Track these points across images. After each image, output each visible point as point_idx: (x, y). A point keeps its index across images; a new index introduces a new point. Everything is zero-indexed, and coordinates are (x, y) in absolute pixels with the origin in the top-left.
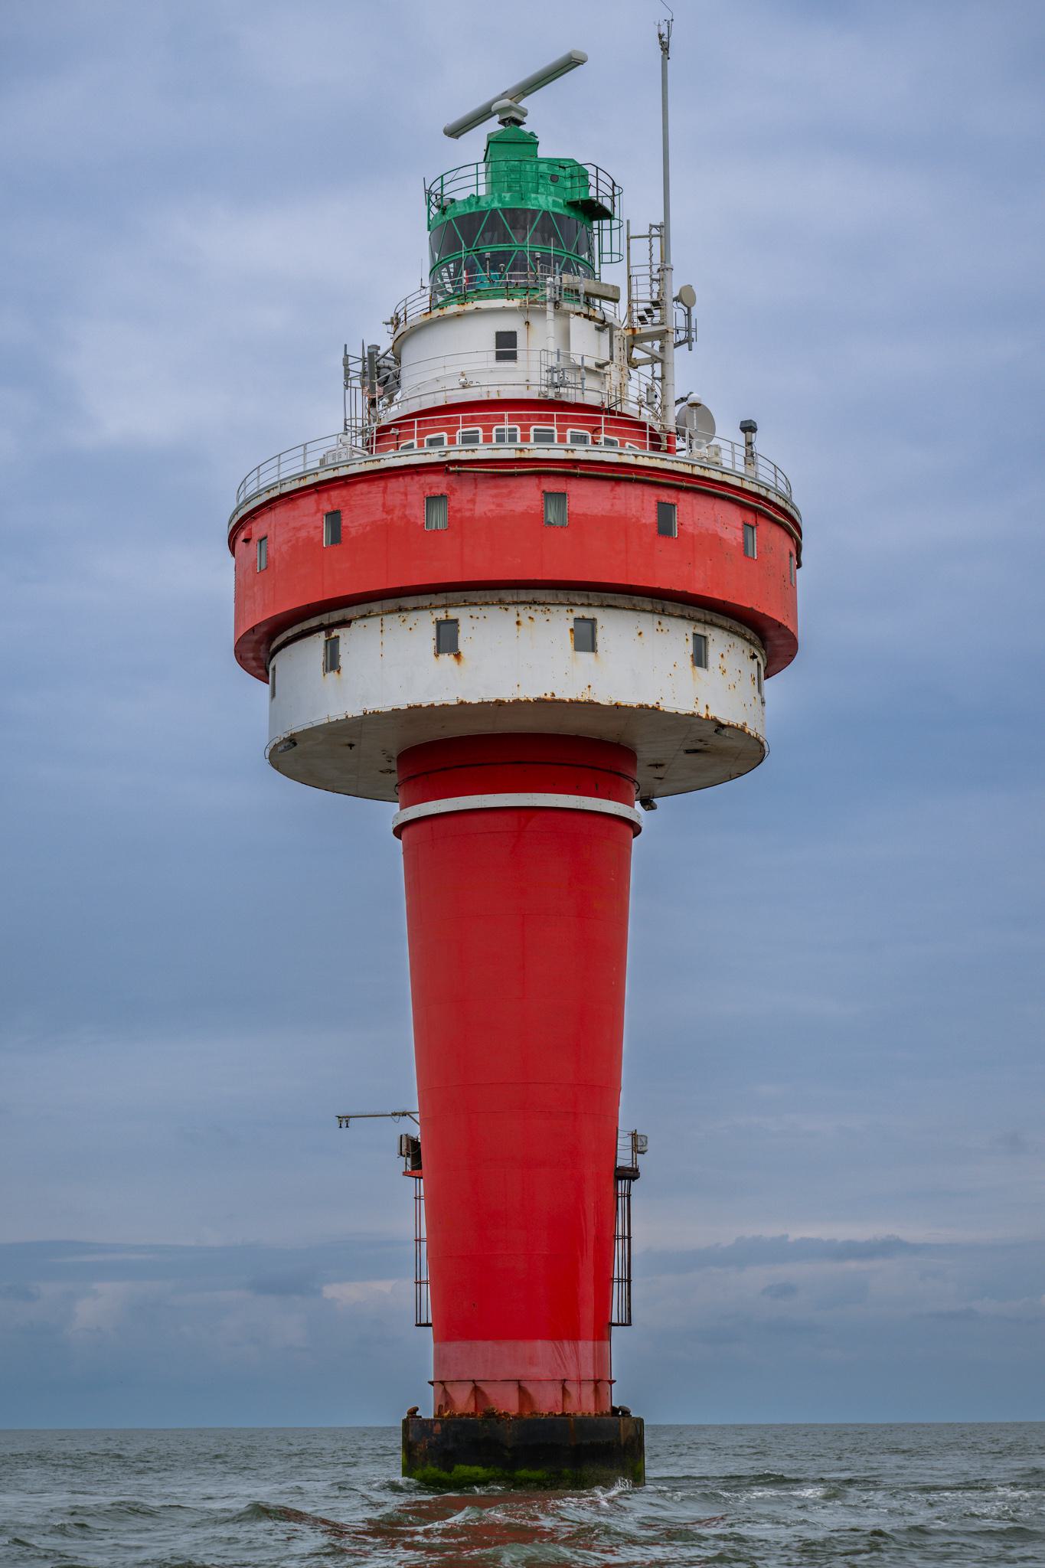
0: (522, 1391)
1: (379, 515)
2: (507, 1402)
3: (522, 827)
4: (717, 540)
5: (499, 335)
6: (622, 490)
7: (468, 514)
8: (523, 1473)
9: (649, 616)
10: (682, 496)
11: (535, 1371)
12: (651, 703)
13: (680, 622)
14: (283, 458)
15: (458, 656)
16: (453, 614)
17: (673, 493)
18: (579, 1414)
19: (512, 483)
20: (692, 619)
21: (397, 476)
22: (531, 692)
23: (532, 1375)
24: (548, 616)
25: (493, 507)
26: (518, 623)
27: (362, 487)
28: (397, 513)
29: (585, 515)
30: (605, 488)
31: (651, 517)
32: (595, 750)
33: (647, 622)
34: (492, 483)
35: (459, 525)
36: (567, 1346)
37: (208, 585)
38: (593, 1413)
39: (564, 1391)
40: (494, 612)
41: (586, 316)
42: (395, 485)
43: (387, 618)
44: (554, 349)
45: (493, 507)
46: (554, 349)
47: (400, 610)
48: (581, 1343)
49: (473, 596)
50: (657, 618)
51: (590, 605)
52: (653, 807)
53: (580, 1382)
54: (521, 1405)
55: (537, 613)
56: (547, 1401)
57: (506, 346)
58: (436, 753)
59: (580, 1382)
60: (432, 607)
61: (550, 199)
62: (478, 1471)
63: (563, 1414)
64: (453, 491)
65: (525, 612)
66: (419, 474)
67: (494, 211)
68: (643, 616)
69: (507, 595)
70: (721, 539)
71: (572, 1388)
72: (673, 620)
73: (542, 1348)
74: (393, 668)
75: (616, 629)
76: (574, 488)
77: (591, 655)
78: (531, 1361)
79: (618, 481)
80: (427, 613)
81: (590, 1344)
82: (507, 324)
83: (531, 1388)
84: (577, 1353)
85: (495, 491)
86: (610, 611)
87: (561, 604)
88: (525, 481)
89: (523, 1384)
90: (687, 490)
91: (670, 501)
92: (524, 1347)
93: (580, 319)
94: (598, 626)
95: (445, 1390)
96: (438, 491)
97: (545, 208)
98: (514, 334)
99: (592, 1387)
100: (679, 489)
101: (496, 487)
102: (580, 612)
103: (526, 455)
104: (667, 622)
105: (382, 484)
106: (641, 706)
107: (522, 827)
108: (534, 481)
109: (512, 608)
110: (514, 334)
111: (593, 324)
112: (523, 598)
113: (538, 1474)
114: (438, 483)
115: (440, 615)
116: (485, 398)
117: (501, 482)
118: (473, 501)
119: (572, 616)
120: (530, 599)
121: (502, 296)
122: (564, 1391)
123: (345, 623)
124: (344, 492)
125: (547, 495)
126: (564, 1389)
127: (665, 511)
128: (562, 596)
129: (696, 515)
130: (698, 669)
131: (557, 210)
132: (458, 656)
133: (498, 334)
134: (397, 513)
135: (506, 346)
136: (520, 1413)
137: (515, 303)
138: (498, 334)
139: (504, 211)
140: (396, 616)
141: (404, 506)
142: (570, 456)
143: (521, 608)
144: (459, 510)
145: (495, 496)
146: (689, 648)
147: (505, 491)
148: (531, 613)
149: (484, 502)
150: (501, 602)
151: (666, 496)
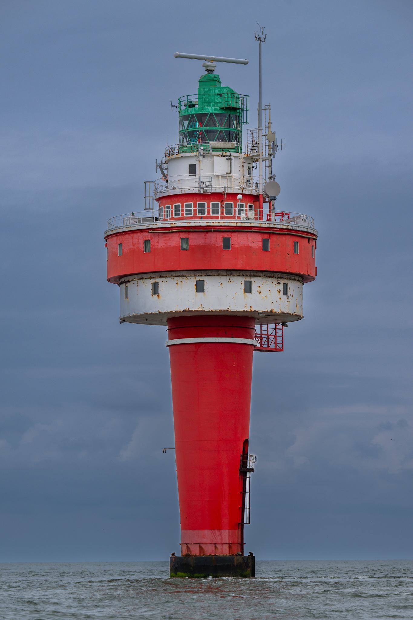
0: (200, 547)
1: (131, 247)
2: (196, 551)
3: (215, 349)
4: (248, 248)
5: (190, 166)
6: (208, 235)
7: (156, 247)
8: (196, 575)
9: (225, 277)
10: (233, 234)
11: (205, 541)
12: (225, 309)
13: (239, 277)
14: (148, 195)
15: (158, 296)
16: (157, 280)
17: (229, 234)
18: (222, 555)
19: (170, 235)
20: (243, 276)
21: (136, 233)
22: (181, 309)
23: (215, 542)
24: (187, 280)
25: (164, 244)
26: (177, 283)
27: (127, 236)
28: (136, 246)
29: (195, 245)
30: (203, 235)
31: (220, 243)
32: (238, 322)
33: (224, 280)
34: (164, 235)
35: (154, 251)
36: (217, 532)
37: (98, 262)
38: (228, 555)
39: (216, 547)
40: (169, 280)
41: (221, 156)
42: (136, 235)
43: (139, 281)
44: (218, 171)
45: (164, 244)
46: (218, 171)
47: (142, 278)
48: (223, 531)
49: (163, 274)
50: (228, 277)
51: (201, 276)
52: (286, 326)
53: (222, 544)
54: (200, 552)
55: (183, 280)
56: (209, 550)
57: (192, 170)
58: (183, 323)
59: (222, 544)
60: (151, 278)
61: (213, 108)
62: (183, 574)
63: (215, 555)
64: (152, 238)
65: (179, 279)
66: (142, 232)
67: (193, 115)
68: (222, 277)
69: (174, 274)
70: (250, 247)
71: (219, 546)
72: (235, 277)
73: (207, 532)
74: (179, 296)
75: (210, 283)
76: (191, 236)
77: (202, 293)
78: (204, 537)
79: (207, 232)
80: (149, 280)
81: (228, 531)
82: (193, 162)
83: (203, 546)
84: (221, 534)
85: (165, 238)
86: (209, 277)
87: (191, 276)
88: (174, 235)
89: (201, 545)
90: (235, 232)
91: (227, 237)
92: (201, 532)
93: (220, 157)
94: (205, 283)
95: (187, 546)
96: (147, 239)
97: (211, 112)
98: (195, 165)
99: (228, 546)
100: (231, 232)
101: (165, 237)
102: (198, 278)
103: (173, 226)
104: (232, 278)
105: (132, 235)
106: (221, 310)
107: (215, 349)
108: (177, 234)
109: (175, 278)
110: (195, 165)
111: (225, 158)
112: (179, 275)
113: (202, 575)
114: (147, 236)
115: (153, 281)
116: (180, 193)
117: (167, 235)
118: (158, 242)
119: (195, 280)
120: (181, 275)
121: (190, 151)
122: (216, 547)
123: (129, 282)
124: (123, 237)
125: (182, 239)
126: (215, 546)
127: (227, 243)
128: (192, 273)
129: (238, 240)
130: (247, 294)
131: (216, 112)
132: (158, 296)
133: (190, 165)
134: (136, 246)
135: (192, 170)
136: (200, 555)
137: (194, 154)
138: (190, 165)
139: (196, 114)
140: (141, 280)
141: (138, 244)
142: (189, 225)
143: (178, 278)
144: (154, 246)
145: (165, 240)
146: (243, 286)
147: (168, 238)
148: (181, 280)
149: (161, 242)
150: (171, 276)
151: (226, 235)
